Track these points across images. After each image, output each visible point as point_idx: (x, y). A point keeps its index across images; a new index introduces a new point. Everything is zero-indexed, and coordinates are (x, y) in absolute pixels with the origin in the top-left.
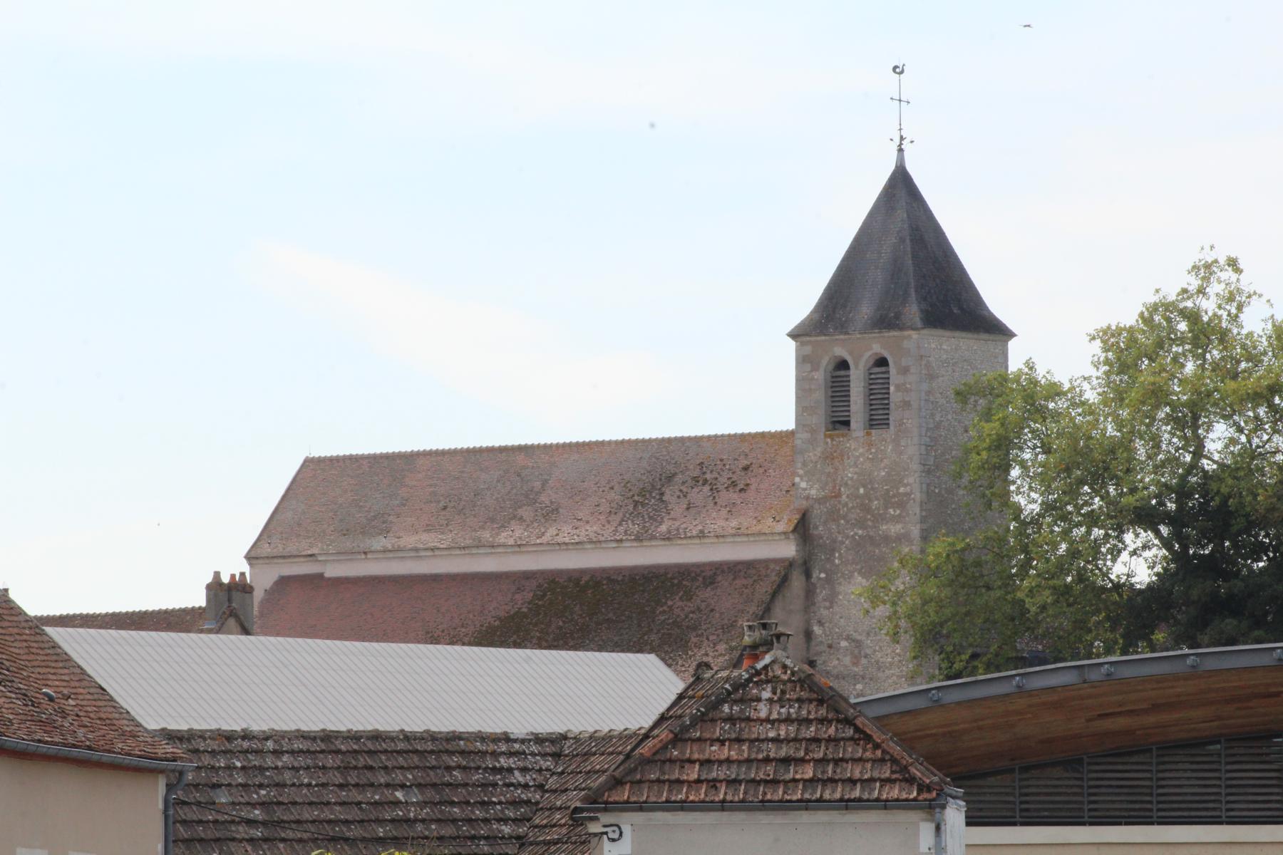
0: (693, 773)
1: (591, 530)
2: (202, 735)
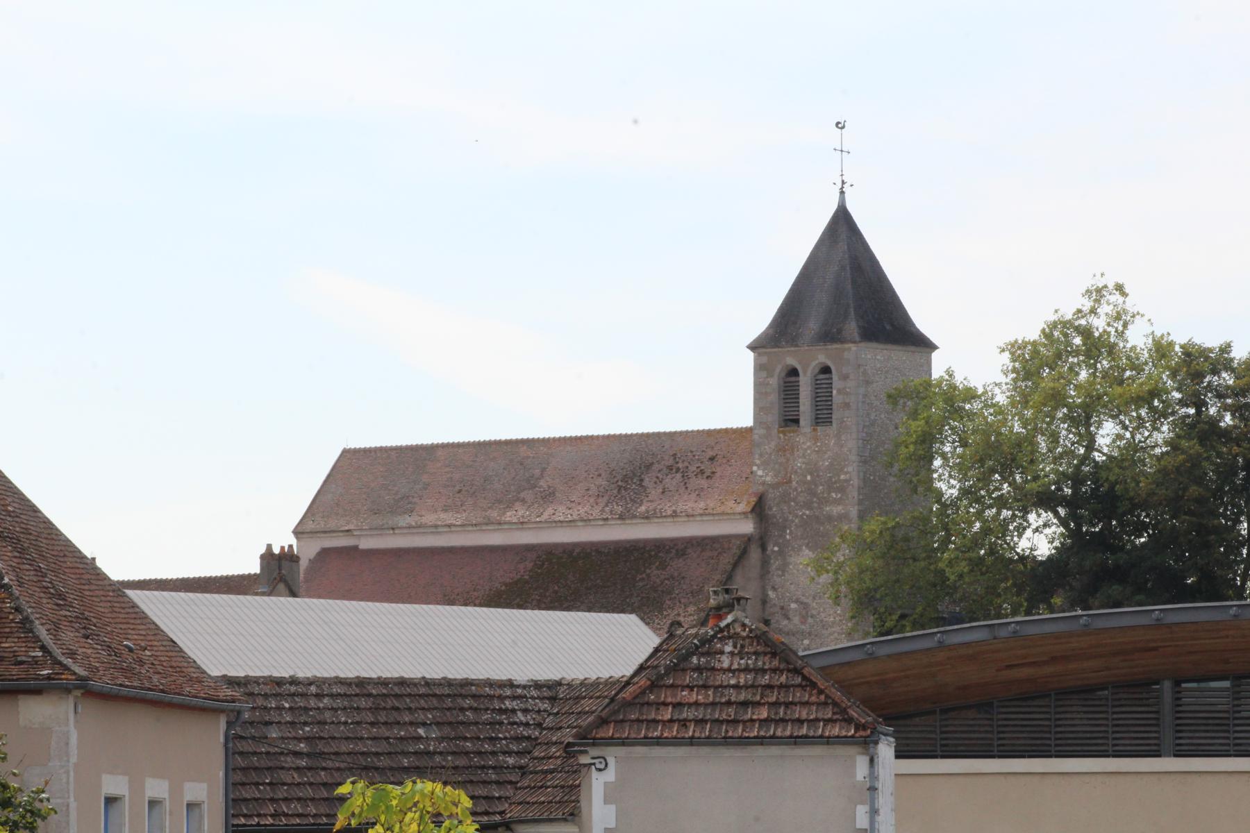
0: (667, 714)
2: (256, 681)
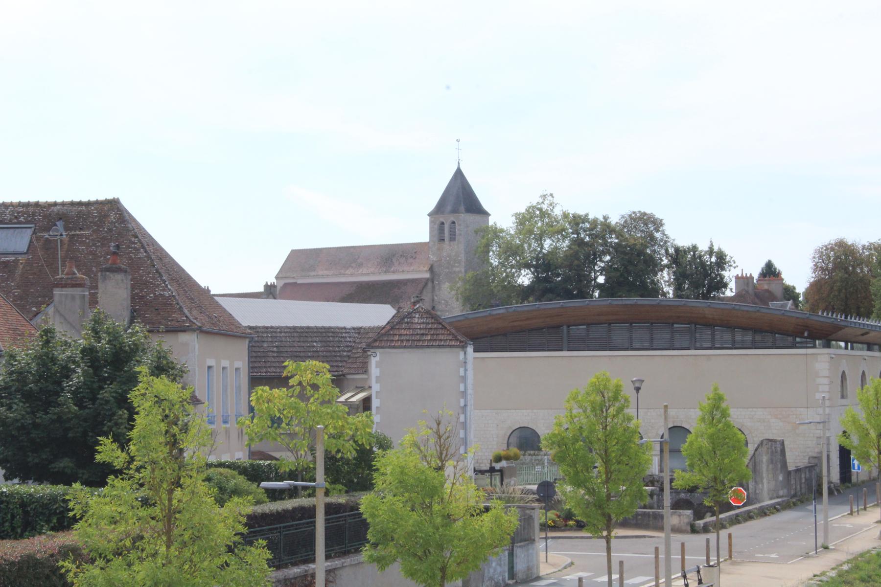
0: (397, 338)
1: (372, 270)
2: (259, 327)
